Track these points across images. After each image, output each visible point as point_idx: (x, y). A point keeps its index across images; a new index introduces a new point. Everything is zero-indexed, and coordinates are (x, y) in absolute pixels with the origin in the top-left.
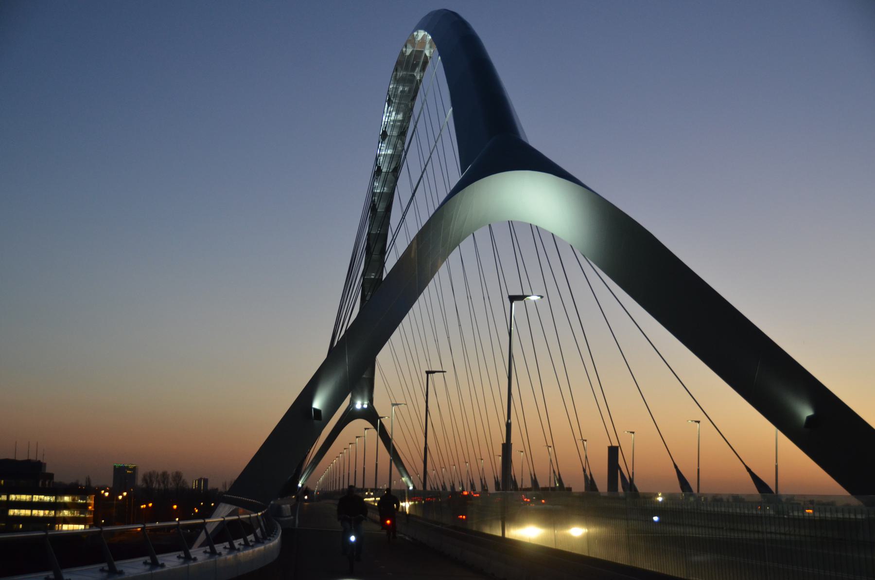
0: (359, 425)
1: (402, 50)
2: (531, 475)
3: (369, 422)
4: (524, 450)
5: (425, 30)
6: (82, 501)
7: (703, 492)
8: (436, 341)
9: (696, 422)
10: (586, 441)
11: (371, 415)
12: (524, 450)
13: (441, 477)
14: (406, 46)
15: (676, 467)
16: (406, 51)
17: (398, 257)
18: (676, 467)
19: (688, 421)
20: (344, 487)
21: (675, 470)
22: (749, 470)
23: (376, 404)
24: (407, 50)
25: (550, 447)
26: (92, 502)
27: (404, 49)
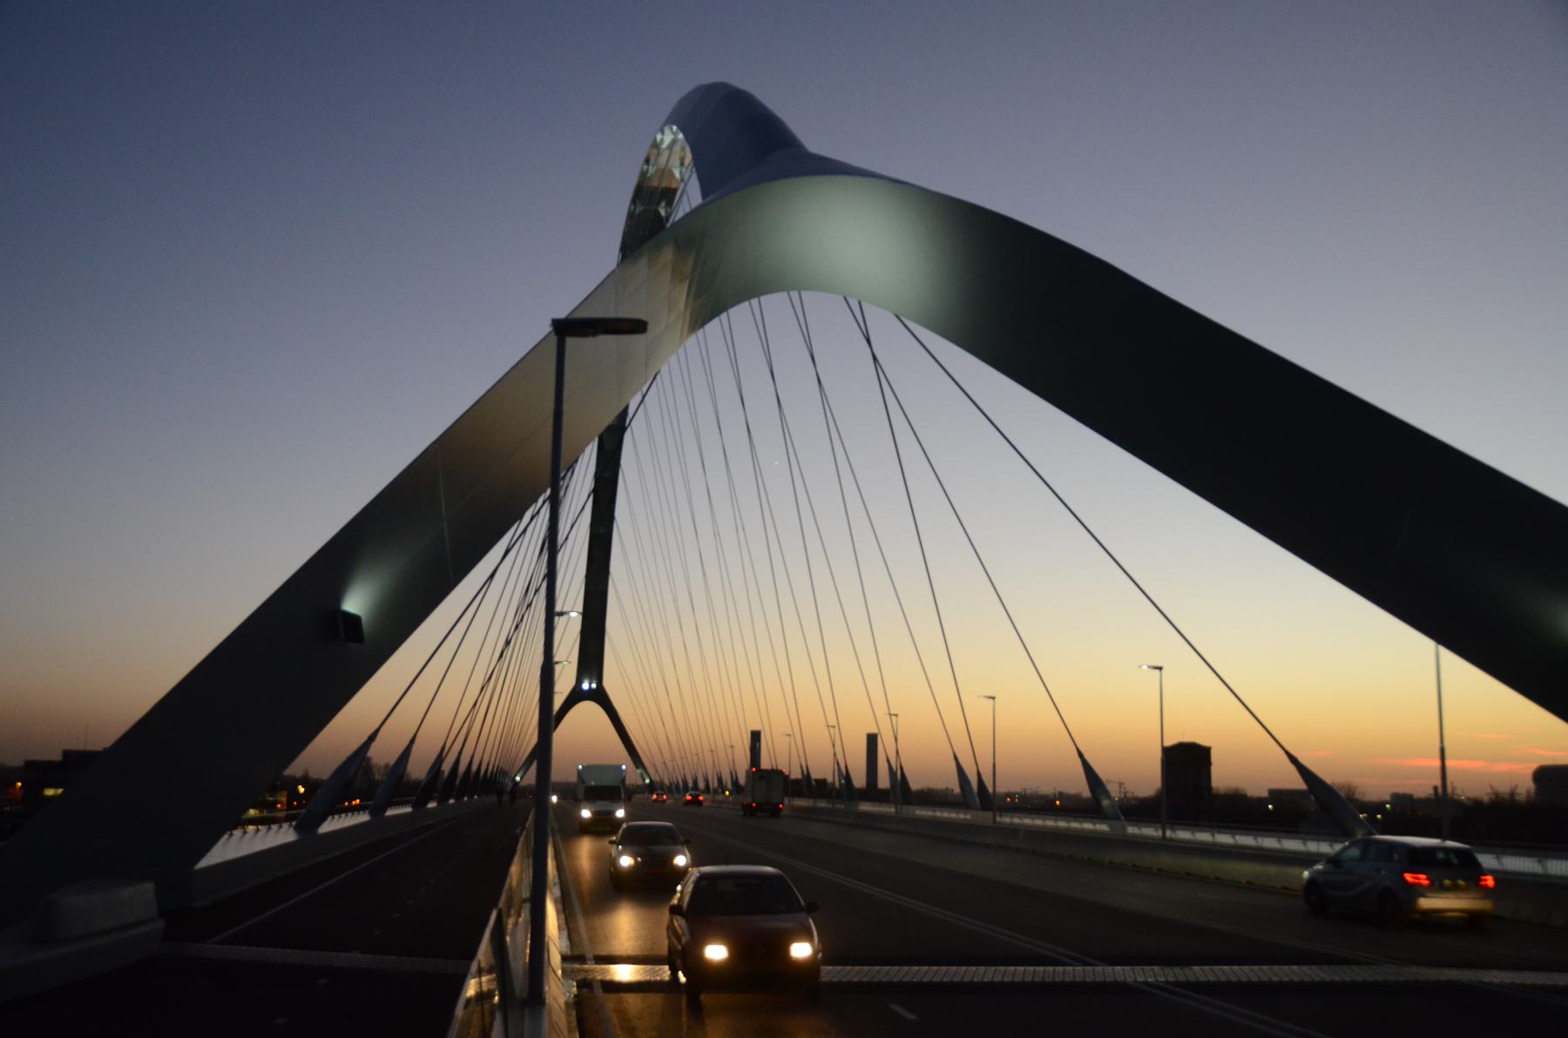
0: (588, 711)
1: (655, 139)
2: (801, 767)
3: (603, 708)
4: (791, 733)
5: (682, 129)
6: (271, 799)
7: (559, 780)
8: (675, 600)
9: (990, 698)
10: (896, 715)
11: (600, 697)
12: (836, 724)
13: (681, 767)
14: (662, 132)
15: (1081, 755)
16: (662, 140)
17: (659, 383)
18: (1081, 755)
19: (1140, 667)
20: (675, 355)
21: (954, 762)
22: (1293, 760)
23: (606, 684)
24: (665, 137)
25: (834, 727)
26: (284, 799)
27: (659, 137)
